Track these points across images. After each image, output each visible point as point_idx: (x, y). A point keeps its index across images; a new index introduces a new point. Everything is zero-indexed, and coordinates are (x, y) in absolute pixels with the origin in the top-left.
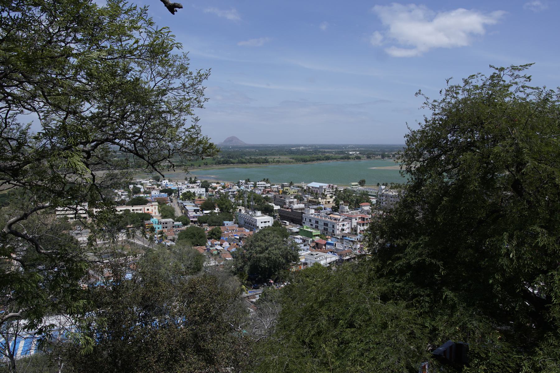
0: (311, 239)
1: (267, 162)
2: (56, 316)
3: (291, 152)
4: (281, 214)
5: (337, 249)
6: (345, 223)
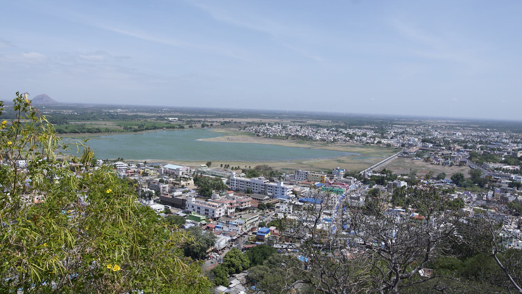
0: (199, 223)
1: (100, 132)
2: (517, 247)
3: (112, 117)
4: (163, 199)
5: (224, 231)
6: (221, 209)
